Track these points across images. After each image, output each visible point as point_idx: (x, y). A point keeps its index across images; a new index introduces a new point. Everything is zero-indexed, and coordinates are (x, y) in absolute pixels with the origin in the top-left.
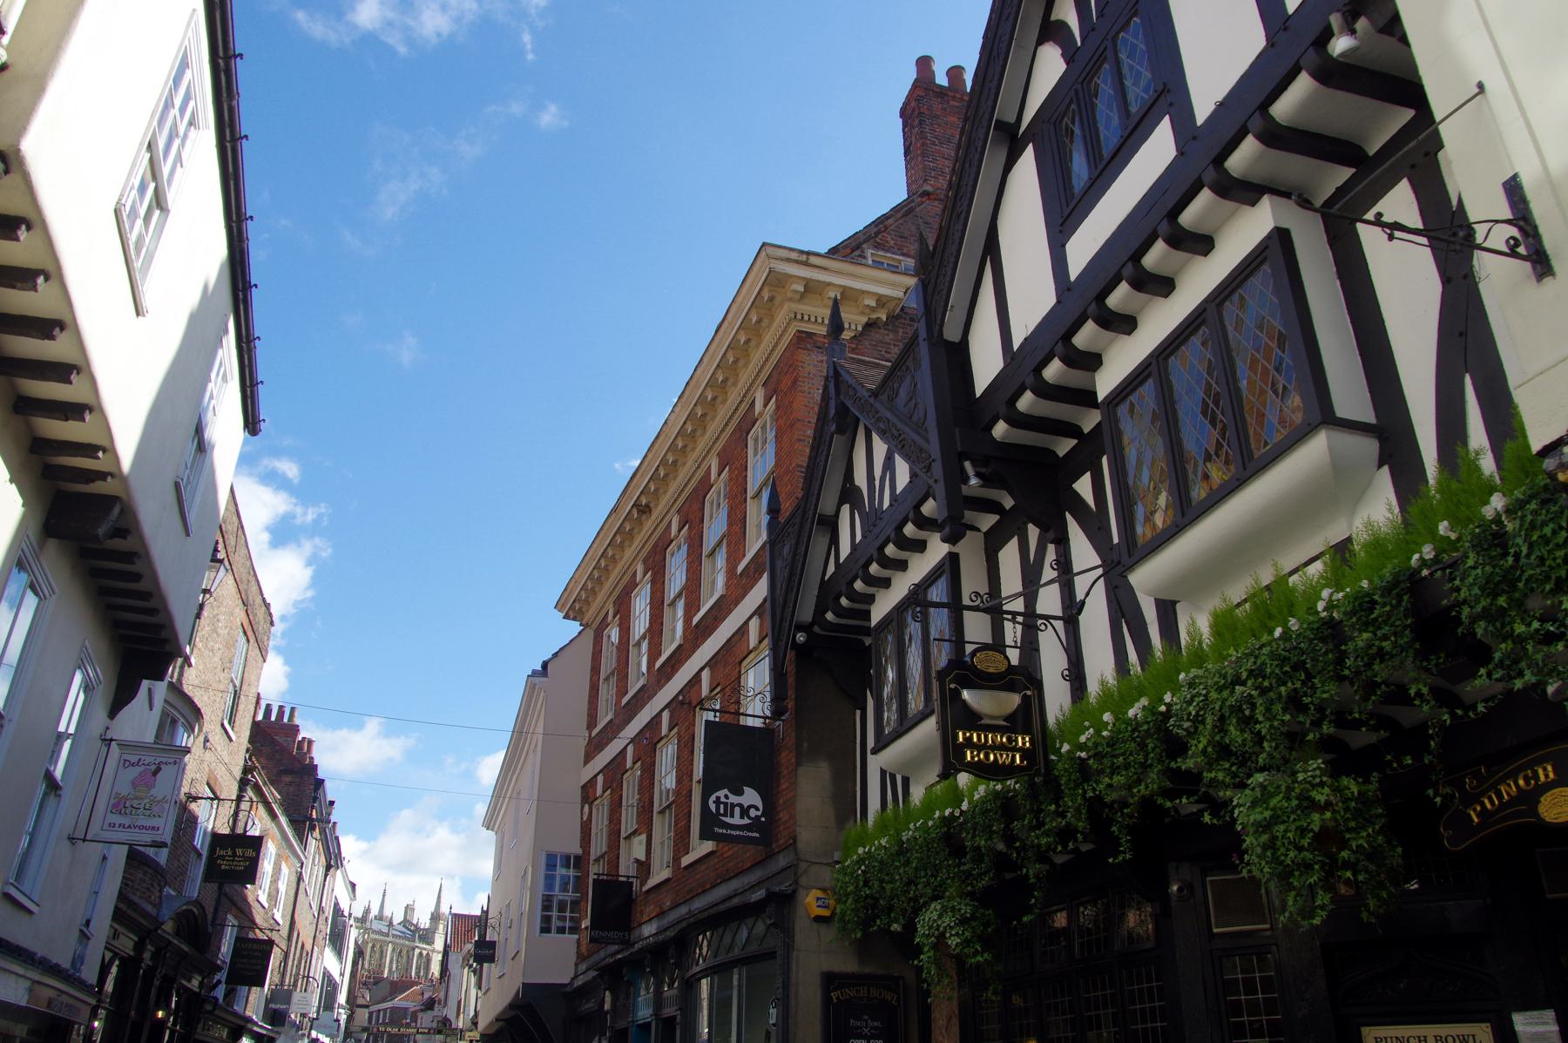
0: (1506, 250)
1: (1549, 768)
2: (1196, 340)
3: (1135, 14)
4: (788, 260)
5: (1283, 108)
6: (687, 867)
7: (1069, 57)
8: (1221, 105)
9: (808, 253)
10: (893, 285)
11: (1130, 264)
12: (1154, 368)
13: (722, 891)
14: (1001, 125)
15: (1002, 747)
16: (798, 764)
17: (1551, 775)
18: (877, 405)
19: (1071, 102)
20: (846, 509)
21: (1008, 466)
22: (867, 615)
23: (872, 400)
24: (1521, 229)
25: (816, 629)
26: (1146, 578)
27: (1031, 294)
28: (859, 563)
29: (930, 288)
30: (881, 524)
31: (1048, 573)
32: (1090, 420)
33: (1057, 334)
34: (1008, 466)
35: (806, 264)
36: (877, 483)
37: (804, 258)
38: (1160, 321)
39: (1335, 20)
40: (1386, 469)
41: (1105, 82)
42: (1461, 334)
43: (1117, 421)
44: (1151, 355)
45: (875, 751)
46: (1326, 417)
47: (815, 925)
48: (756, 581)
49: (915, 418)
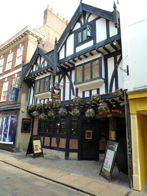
2: (89, 64)
5: (106, 46)
7: (82, 26)
14: (70, 30)
20: (35, 66)
22: (35, 78)
25: (27, 78)
27: (70, 51)
36: (41, 64)
39: (115, 41)
40: (104, 83)
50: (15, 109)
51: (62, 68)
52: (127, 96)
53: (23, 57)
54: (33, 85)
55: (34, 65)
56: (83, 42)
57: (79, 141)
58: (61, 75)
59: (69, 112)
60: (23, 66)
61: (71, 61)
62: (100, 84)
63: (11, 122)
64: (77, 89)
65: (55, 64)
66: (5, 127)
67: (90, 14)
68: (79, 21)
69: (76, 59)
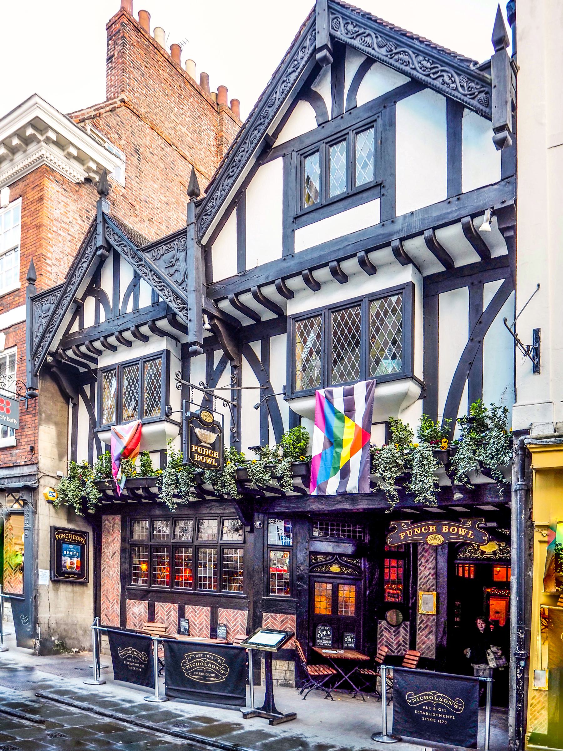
22: (95, 361)
27: (265, 242)
39: (488, 213)
40: (421, 401)
50: (17, 490)
51: (228, 321)
52: (526, 455)
53: (22, 255)
54: (87, 389)
55: (83, 299)
56: (328, 206)
58: (218, 355)
60: (33, 299)
61: (270, 292)
62: (401, 400)
64: (296, 419)
65: (195, 300)
67: (369, 62)
68: (306, 92)
69: (295, 283)
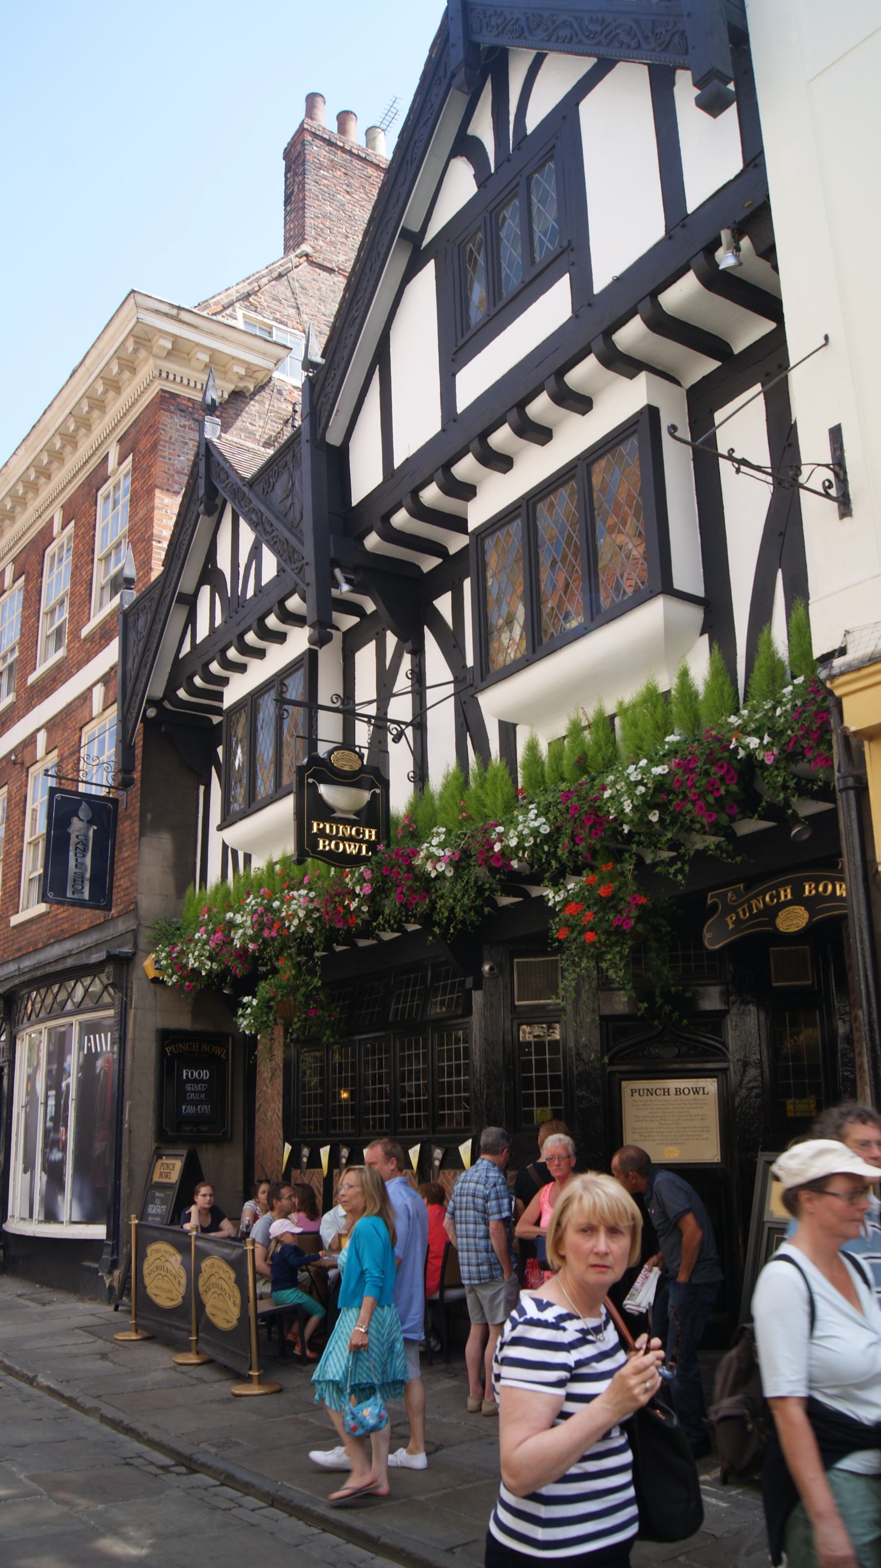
0: (823, 492)
1: (789, 891)
2: (564, 492)
3: (550, 159)
4: (157, 312)
6: (15, 927)
7: (482, 178)
8: (618, 280)
9: (179, 308)
10: (264, 354)
11: (509, 402)
12: (523, 511)
13: (56, 951)
14: (406, 234)
15: (351, 839)
16: (142, 834)
17: (789, 897)
18: (251, 496)
19: (479, 229)
20: (206, 590)
21: (375, 574)
22: (219, 697)
23: (246, 489)
24: (836, 475)
26: (494, 703)
27: (417, 422)
28: (216, 645)
29: (318, 387)
30: (243, 612)
31: (403, 682)
32: (456, 543)
33: (437, 461)
34: (375, 574)
35: (176, 319)
37: (174, 312)
38: (535, 466)
39: (725, 235)
40: (706, 637)
41: (513, 218)
42: (781, 534)
43: (484, 553)
44: (522, 498)
45: (220, 828)
46: (667, 588)
47: (152, 985)
48: (102, 647)
49: (290, 517)
57: (782, 1147)
59: (375, 942)
63: (82, 1068)
66: (51, 1111)
69: (466, 467)
